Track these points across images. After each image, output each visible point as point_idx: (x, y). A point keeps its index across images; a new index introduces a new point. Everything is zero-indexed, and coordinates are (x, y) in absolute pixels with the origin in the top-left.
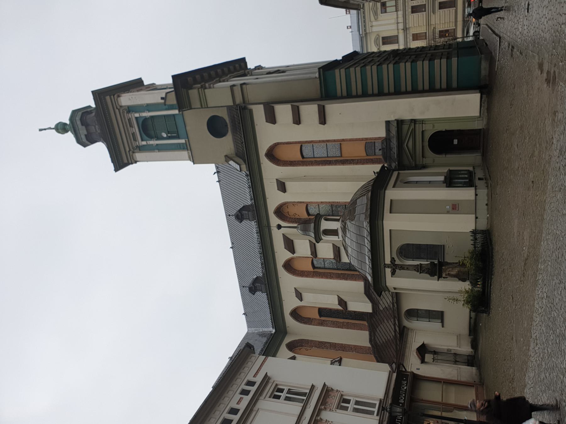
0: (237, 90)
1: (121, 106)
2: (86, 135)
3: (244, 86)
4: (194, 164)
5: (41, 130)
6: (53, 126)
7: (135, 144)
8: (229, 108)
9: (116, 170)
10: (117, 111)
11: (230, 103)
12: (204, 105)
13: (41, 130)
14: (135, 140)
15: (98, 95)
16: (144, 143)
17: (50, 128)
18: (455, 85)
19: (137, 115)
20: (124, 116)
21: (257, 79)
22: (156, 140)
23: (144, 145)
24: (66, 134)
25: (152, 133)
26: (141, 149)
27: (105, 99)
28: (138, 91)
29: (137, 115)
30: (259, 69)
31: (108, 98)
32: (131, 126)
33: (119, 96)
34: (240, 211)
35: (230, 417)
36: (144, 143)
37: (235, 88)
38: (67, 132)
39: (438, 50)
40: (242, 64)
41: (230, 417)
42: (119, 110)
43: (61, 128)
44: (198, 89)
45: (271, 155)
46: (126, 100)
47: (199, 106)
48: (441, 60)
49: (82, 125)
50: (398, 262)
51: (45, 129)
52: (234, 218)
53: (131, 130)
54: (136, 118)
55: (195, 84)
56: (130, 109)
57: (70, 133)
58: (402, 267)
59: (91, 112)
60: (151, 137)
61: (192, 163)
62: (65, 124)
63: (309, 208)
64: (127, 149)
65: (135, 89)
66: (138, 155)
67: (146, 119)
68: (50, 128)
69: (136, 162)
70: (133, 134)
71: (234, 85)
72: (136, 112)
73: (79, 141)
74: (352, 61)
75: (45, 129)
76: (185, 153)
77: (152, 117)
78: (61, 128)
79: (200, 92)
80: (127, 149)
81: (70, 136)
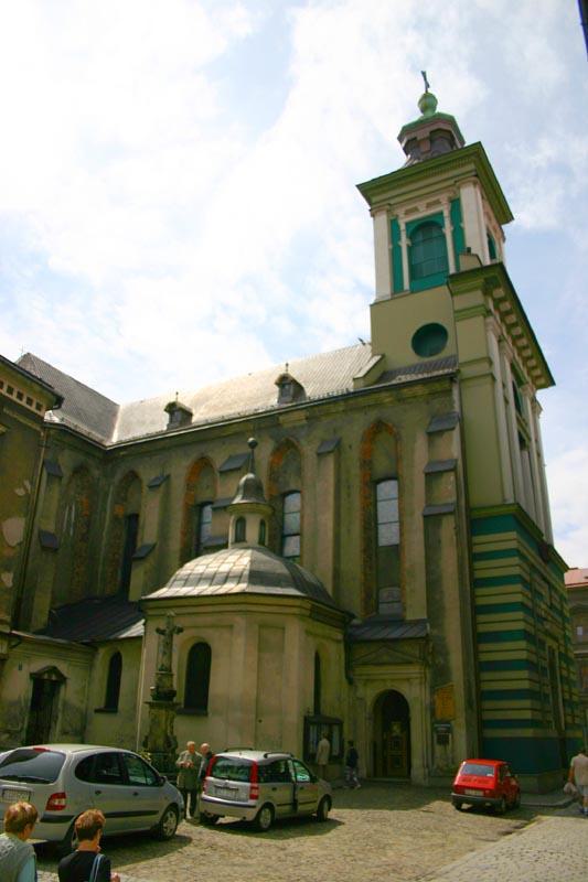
0: (483, 368)
1: (459, 188)
2: (415, 138)
3: (489, 379)
4: (371, 306)
5: (424, 74)
6: (430, 91)
7: (400, 212)
8: (455, 357)
9: (359, 187)
10: (452, 182)
11: (462, 359)
12: (460, 315)
13: (424, 74)
14: (408, 213)
15: (478, 149)
16: (403, 227)
17: (427, 86)
18: (490, 733)
19: (446, 213)
20: (441, 193)
21: (506, 401)
22: (408, 246)
23: (398, 226)
24: (418, 109)
25: (420, 238)
26: (393, 224)
27: (469, 163)
28: (486, 214)
29: (446, 213)
30: (533, 408)
31: (471, 167)
32: (429, 206)
33: (475, 184)
34: (294, 382)
35: (5, 388)
36: (403, 227)
37: (486, 365)
38: (423, 111)
39: (564, 705)
40: (542, 381)
41: (5, 388)
42: (454, 185)
43: (428, 102)
44: (483, 305)
45: (379, 427)
46: (471, 197)
47: (457, 308)
48: (531, 709)
49: (431, 132)
50: (177, 639)
51: (425, 79)
52: (282, 372)
53: (421, 205)
54: (441, 213)
55: (494, 300)
56: (455, 204)
57: (421, 115)
58: (168, 645)
59: (452, 142)
60: (411, 236)
61: (372, 302)
62: (434, 108)
63: (295, 495)
64: (392, 202)
65: (489, 209)
66: (383, 218)
67: (440, 226)
68: (427, 86)
69: (373, 215)
70: (416, 210)
71: (491, 363)
72: (451, 212)
73: (406, 131)
74: (541, 561)
75: (425, 79)
76: (387, 291)
77: (444, 236)
78: (428, 102)
79: (479, 309)
80: (392, 202)
81: (416, 115)
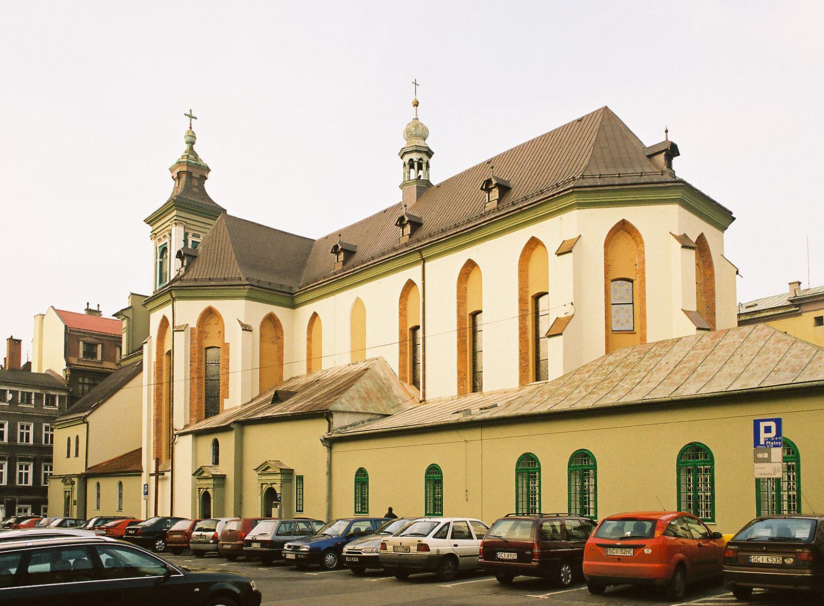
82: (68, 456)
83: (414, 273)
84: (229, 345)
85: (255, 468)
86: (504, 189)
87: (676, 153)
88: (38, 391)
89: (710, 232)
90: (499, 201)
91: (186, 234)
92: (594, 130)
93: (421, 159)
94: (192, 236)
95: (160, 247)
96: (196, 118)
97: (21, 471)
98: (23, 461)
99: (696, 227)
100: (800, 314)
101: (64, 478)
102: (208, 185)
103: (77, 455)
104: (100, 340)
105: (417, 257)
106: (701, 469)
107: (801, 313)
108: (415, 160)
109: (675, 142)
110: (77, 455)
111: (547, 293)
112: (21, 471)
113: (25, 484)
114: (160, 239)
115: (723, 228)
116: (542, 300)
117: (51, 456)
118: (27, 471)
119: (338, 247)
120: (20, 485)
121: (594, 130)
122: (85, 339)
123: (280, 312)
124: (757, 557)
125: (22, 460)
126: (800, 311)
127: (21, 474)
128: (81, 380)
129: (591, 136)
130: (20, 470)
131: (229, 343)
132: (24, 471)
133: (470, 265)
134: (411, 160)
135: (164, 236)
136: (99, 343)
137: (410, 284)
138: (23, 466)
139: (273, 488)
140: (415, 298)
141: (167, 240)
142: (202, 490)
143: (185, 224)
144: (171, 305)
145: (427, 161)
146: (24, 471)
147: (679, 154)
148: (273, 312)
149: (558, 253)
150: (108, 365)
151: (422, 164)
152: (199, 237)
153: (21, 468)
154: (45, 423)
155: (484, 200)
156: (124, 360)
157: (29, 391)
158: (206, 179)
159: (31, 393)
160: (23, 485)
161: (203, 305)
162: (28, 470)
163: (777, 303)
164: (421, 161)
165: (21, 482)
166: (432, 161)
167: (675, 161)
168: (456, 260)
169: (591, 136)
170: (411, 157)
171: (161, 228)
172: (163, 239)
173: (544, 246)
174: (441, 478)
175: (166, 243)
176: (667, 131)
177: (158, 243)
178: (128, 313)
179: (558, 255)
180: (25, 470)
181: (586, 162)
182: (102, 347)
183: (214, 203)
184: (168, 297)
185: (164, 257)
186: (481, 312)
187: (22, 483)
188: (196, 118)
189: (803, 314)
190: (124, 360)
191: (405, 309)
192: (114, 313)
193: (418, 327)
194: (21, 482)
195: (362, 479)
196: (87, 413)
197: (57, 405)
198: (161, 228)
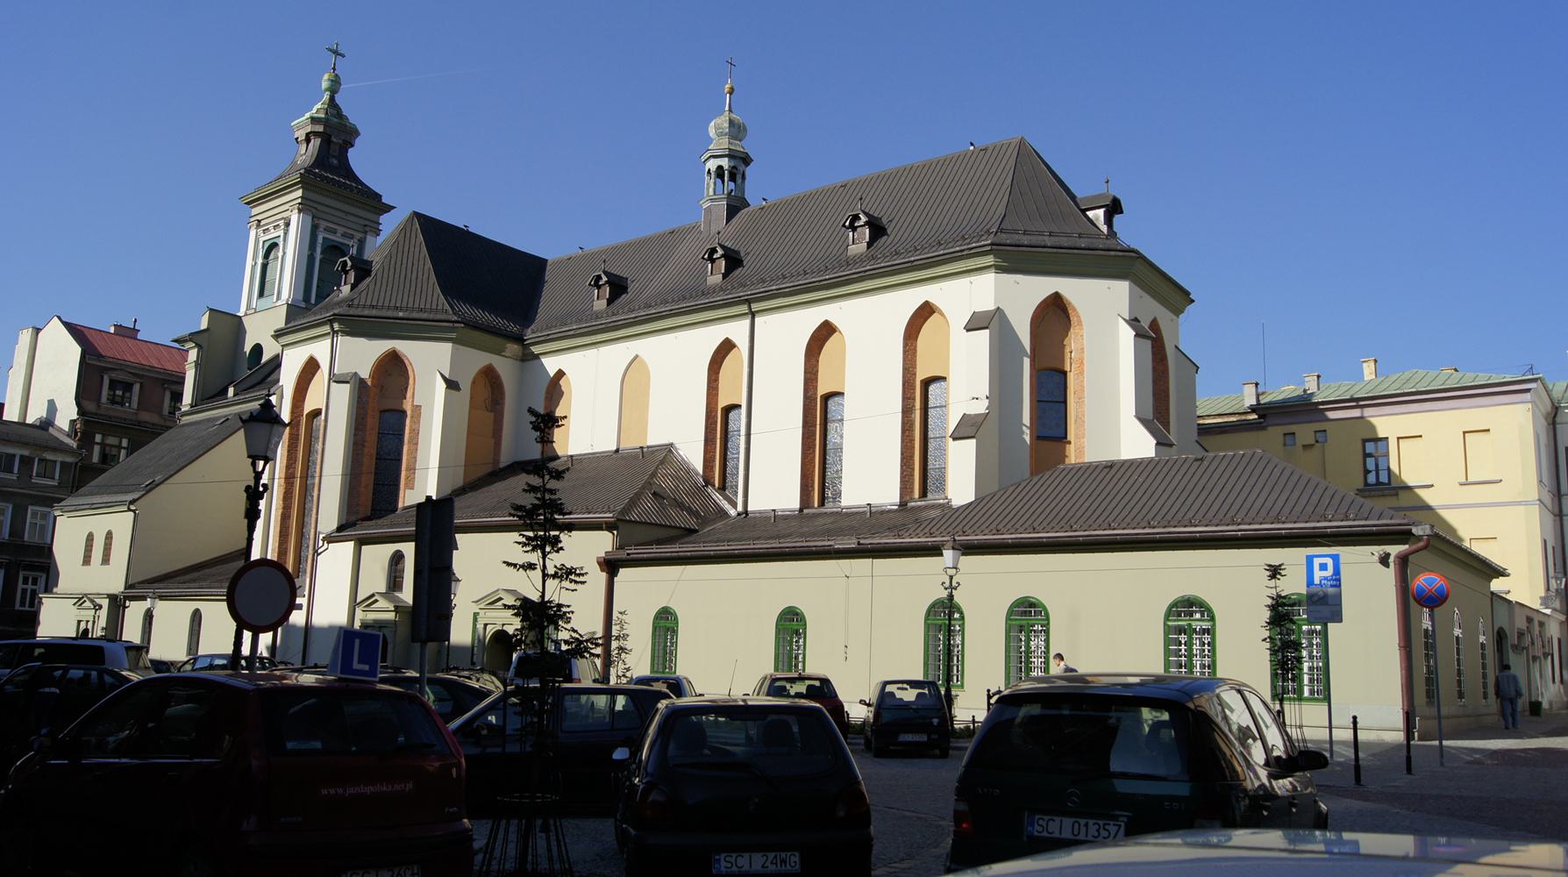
80: (259, 218)
82: (87, 560)
83: (737, 330)
84: (420, 410)
85: (475, 599)
86: (877, 230)
87: (1119, 211)
88: (26, 453)
89: (1163, 315)
90: (870, 245)
91: (315, 228)
92: (1008, 168)
93: (734, 167)
94: (325, 229)
95: (264, 242)
96: (343, 56)
97: (25, 586)
98: (29, 570)
99: (1153, 309)
100: (1264, 428)
101: (80, 599)
102: (351, 153)
103: (106, 560)
104: (141, 377)
105: (744, 308)
106: (360, 662)
107: (1266, 427)
108: (726, 167)
109: (1118, 197)
110: (106, 560)
111: (944, 379)
112: (25, 586)
113: (29, 607)
114: (268, 229)
115: (1178, 311)
116: (933, 389)
117: (49, 561)
118: (34, 587)
119: (601, 278)
120: (21, 609)
121: (1008, 168)
122: (113, 375)
123: (504, 366)
124: (1046, 818)
125: (27, 567)
126: (1265, 424)
127: (24, 591)
128: (98, 438)
129: (1004, 176)
130: (23, 584)
131: (420, 406)
132: (30, 587)
133: (826, 331)
134: (720, 168)
135: (275, 226)
136: (136, 382)
137: (727, 347)
138: (28, 578)
139: (504, 631)
140: (734, 366)
141: (281, 233)
142: (489, 627)
143: (314, 211)
144: (329, 341)
145: (744, 172)
146: (30, 587)
147: (1122, 212)
148: (493, 364)
149: (967, 328)
150: (146, 417)
151: (735, 174)
152: (335, 233)
153: (25, 581)
154: (32, 505)
155: (845, 236)
156: (186, 414)
157: (10, 450)
158: (352, 146)
159: (14, 456)
160: (27, 608)
161: (382, 346)
162: (36, 585)
163: (1227, 407)
164: (734, 171)
165: (23, 604)
166: (749, 171)
167: (1117, 219)
168: (806, 320)
169: (1004, 176)
170: (720, 163)
171: (276, 211)
172: (273, 231)
173: (945, 317)
174: (1046, 622)
175: (279, 236)
176: (1107, 182)
177: (262, 235)
178: (201, 339)
179: (968, 331)
180: (32, 584)
181: (1001, 210)
182: (141, 387)
183: (362, 184)
184: (327, 329)
185: (272, 256)
186: (841, 394)
187: (24, 606)
188: (343, 56)
189: (1269, 428)
190: (186, 414)
191: (717, 380)
192: (175, 337)
193: (738, 406)
194: (23, 604)
195: (665, 624)
196: (136, 496)
197: (57, 476)
198: (276, 211)
